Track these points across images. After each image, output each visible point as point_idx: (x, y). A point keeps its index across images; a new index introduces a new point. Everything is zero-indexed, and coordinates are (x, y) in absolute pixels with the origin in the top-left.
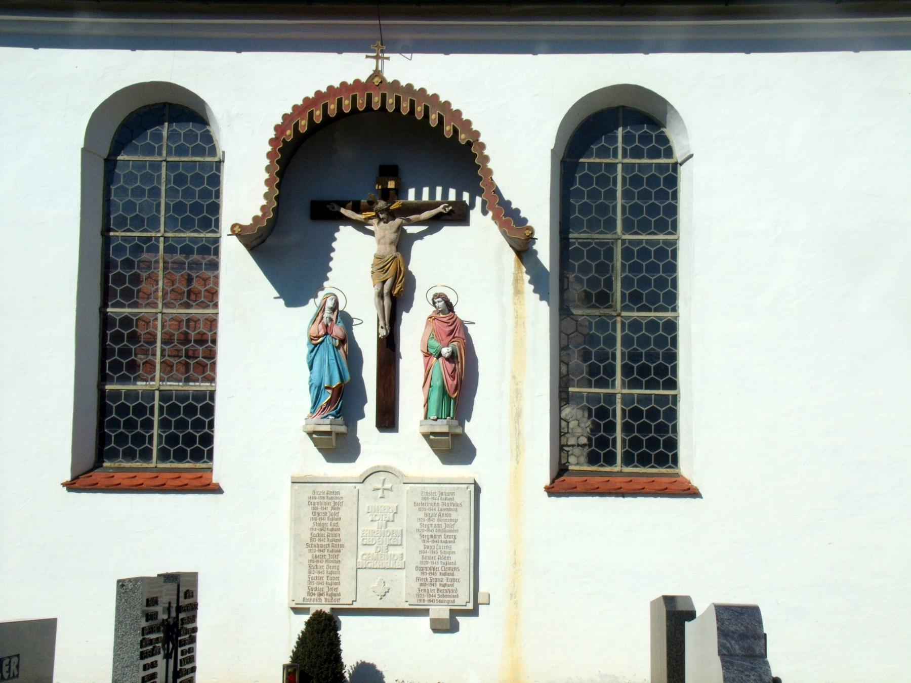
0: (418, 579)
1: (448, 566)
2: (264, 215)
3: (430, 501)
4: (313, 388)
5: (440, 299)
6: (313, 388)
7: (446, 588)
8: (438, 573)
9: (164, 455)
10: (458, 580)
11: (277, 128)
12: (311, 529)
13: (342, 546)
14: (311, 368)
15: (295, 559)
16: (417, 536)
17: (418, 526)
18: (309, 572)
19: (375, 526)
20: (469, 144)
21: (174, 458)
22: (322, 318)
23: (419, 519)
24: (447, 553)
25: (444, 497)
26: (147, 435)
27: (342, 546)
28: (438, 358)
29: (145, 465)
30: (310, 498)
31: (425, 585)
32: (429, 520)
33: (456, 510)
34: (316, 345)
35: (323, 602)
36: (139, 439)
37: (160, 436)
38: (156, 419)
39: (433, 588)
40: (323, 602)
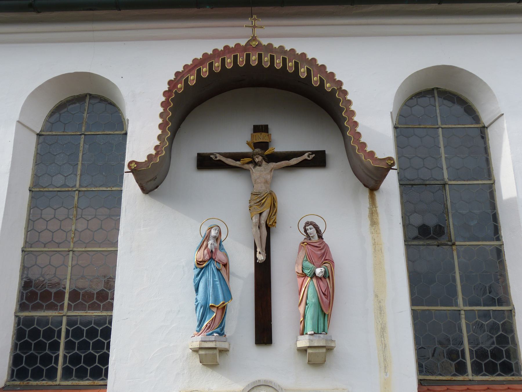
2: (157, 154)
5: (311, 226)
9: (67, 373)
14: (197, 290)
20: (333, 91)
22: (207, 245)
26: (54, 355)
28: (311, 278)
29: (50, 383)
34: (202, 269)
36: (47, 360)
37: (65, 357)
38: (62, 341)
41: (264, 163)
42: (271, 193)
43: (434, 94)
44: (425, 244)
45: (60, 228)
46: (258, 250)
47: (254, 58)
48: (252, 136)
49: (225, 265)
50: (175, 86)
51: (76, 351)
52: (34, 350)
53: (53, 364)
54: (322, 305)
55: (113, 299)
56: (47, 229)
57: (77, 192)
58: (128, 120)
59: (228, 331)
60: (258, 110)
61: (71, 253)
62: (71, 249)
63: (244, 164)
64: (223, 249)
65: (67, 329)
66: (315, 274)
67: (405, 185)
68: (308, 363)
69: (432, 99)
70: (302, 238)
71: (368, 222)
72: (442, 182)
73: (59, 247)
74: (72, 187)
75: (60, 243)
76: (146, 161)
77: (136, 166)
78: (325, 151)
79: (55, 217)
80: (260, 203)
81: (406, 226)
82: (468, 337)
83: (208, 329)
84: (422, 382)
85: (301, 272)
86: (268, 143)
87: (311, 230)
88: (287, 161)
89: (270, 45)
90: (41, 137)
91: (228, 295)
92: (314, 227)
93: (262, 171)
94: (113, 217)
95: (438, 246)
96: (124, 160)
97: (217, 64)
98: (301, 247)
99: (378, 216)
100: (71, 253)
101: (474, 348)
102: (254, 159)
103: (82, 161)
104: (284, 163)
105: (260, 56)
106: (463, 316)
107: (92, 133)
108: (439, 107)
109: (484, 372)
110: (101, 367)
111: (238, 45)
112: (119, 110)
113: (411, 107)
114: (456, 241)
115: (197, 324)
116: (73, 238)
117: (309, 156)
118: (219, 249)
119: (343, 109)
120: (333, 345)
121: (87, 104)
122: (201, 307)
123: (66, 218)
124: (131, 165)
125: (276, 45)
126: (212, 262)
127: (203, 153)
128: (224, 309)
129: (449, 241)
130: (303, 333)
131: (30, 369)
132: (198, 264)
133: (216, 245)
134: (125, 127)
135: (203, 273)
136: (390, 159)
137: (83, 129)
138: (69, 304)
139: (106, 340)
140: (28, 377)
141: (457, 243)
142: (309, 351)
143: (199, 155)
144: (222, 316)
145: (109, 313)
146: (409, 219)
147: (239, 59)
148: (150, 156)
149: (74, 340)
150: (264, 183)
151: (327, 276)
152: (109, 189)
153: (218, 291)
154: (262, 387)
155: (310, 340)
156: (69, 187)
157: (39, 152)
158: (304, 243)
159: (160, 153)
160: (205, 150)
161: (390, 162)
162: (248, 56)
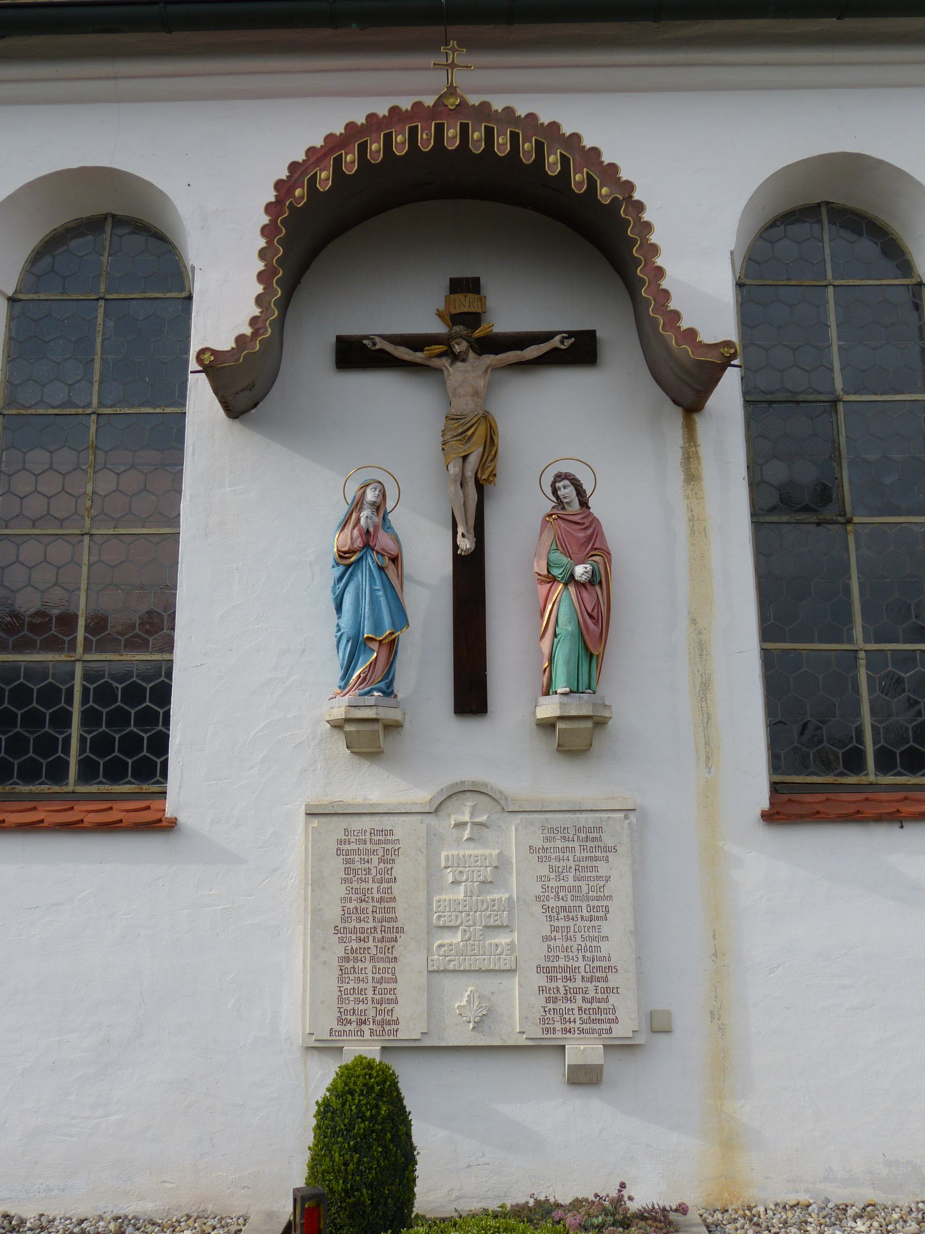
0: (541, 989)
1: (597, 964)
2: (255, 334)
3: (559, 844)
4: (344, 641)
5: (566, 482)
6: (344, 641)
7: (595, 1005)
8: (578, 977)
9: (88, 772)
10: (615, 990)
11: (279, 185)
12: (343, 899)
13: (400, 930)
14: (339, 608)
15: (314, 956)
16: (537, 909)
17: (538, 891)
18: (341, 980)
19: (460, 893)
21: (105, 776)
22: (358, 520)
23: (540, 878)
24: (593, 939)
25: (583, 835)
26: (61, 737)
27: (400, 930)
28: (566, 585)
29: (56, 789)
30: (340, 842)
31: (555, 1000)
32: (558, 878)
33: (607, 860)
34: (348, 566)
35: (367, 1035)
36: (47, 745)
37: (82, 739)
39: (569, 1005)
40: (367, 1035)
41: (471, 354)
42: (486, 417)
43: (820, 215)
44: (792, 520)
45: (63, 489)
46: (460, 530)
47: (452, 133)
48: (447, 301)
49: (395, 560)
50: (290, 192)
51: (104, 728)
52: (21, 727)
53: (60, 754)
54: (586, 637)
55: (173, 629)
56: (36, 491)
57: (94, 417)
58: (193, 268)
59: (402, 687)
60: (460, 241)
61: (87, 538)
62: (86, 531)
63: (430, 357)
64: (390, 527)
65: (84, 686)
66: (572, 576)
67: (756, 403)
68: (558, 750)
69: (816, 227)
70: (548, 505)
71: (676, 475)
72: (831, 397)
73: (61, 527)
74: (84, 407)
75: (64, 519)
76: (233, 349)
77: (212, 358)
78: (595, 331)
79: (51, 468)
80: (464, 437)
81: (755, 485)
82: (870, 701)
83: (361, 684)
84: (778, 787)
85: (545, 573)
86: (479, 314)
87: (567, 491)
88: (519, 352)
89: (485, 105)
90: (17, 306)
91: (401, 617)
92: (573, 484)
93: (469, 372)
94: (168, 468)
95: (818, 524)
96: (187, 351)
97: (374, 147)
98: (545, 523)
99: (700, 464)
100: (87, 538)
101: (880, 723)
102: (450, 347)
103: (102, 353)
104: (512, 356)
105: (464, 128)
106: (862, 662)
107: (121, 296)
108: (828, 242)
109: (899, 769)
110: (154, 758)
111: (418, 105)
112: (175, 248)
113: (772, 243)
114: (853, 515)
115: (340, 673)
116: (89, 510)
117: (562, 342)
118: (383, 528)
119: (635, 241)
120: (607, 714)
121: (107, 236)
122: (348, 641)
123: (74, 470)
124: (202, 357)
125: (498, 104)
126: (368, 554)
127: (348, 337)
128: (392, 645)
129: (840, 515)
130: (547, 691)
131: (16, 762)
132: (340, 557)
133: (376, 519)
134: (186, 284)
135: (351, 575)
136: (728, 344)
137: (102, 287)
138: (86, 638)
139: (161, 707)
140: (12, 777)
141: (856, 520)
142: (560, 725)
143: (340, 339)
144: (388, 659)
145: (166, 657)
146: (761, 471)
147: (422, 136)
148: (241, 340)
149: (99, 708)
150: (473, 396)
151: (597, 581)
152: (158, 410)
153: (380, 609)
154: (468, 795)
155: (562, 705)
156: (79, 407)
157: (13, 335)
158: (551, 515)
159: (261, 331)
160: (353, 329)
161: (727, 352)
162: (440, 129)
